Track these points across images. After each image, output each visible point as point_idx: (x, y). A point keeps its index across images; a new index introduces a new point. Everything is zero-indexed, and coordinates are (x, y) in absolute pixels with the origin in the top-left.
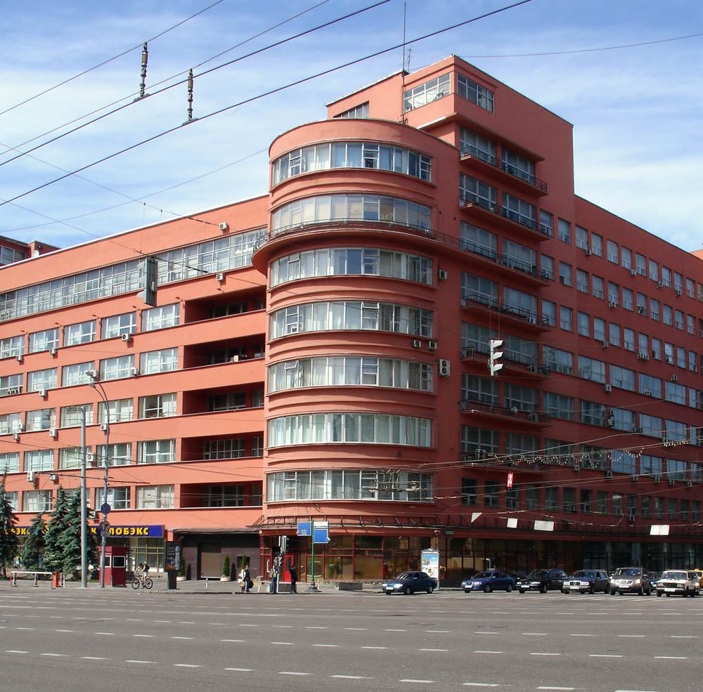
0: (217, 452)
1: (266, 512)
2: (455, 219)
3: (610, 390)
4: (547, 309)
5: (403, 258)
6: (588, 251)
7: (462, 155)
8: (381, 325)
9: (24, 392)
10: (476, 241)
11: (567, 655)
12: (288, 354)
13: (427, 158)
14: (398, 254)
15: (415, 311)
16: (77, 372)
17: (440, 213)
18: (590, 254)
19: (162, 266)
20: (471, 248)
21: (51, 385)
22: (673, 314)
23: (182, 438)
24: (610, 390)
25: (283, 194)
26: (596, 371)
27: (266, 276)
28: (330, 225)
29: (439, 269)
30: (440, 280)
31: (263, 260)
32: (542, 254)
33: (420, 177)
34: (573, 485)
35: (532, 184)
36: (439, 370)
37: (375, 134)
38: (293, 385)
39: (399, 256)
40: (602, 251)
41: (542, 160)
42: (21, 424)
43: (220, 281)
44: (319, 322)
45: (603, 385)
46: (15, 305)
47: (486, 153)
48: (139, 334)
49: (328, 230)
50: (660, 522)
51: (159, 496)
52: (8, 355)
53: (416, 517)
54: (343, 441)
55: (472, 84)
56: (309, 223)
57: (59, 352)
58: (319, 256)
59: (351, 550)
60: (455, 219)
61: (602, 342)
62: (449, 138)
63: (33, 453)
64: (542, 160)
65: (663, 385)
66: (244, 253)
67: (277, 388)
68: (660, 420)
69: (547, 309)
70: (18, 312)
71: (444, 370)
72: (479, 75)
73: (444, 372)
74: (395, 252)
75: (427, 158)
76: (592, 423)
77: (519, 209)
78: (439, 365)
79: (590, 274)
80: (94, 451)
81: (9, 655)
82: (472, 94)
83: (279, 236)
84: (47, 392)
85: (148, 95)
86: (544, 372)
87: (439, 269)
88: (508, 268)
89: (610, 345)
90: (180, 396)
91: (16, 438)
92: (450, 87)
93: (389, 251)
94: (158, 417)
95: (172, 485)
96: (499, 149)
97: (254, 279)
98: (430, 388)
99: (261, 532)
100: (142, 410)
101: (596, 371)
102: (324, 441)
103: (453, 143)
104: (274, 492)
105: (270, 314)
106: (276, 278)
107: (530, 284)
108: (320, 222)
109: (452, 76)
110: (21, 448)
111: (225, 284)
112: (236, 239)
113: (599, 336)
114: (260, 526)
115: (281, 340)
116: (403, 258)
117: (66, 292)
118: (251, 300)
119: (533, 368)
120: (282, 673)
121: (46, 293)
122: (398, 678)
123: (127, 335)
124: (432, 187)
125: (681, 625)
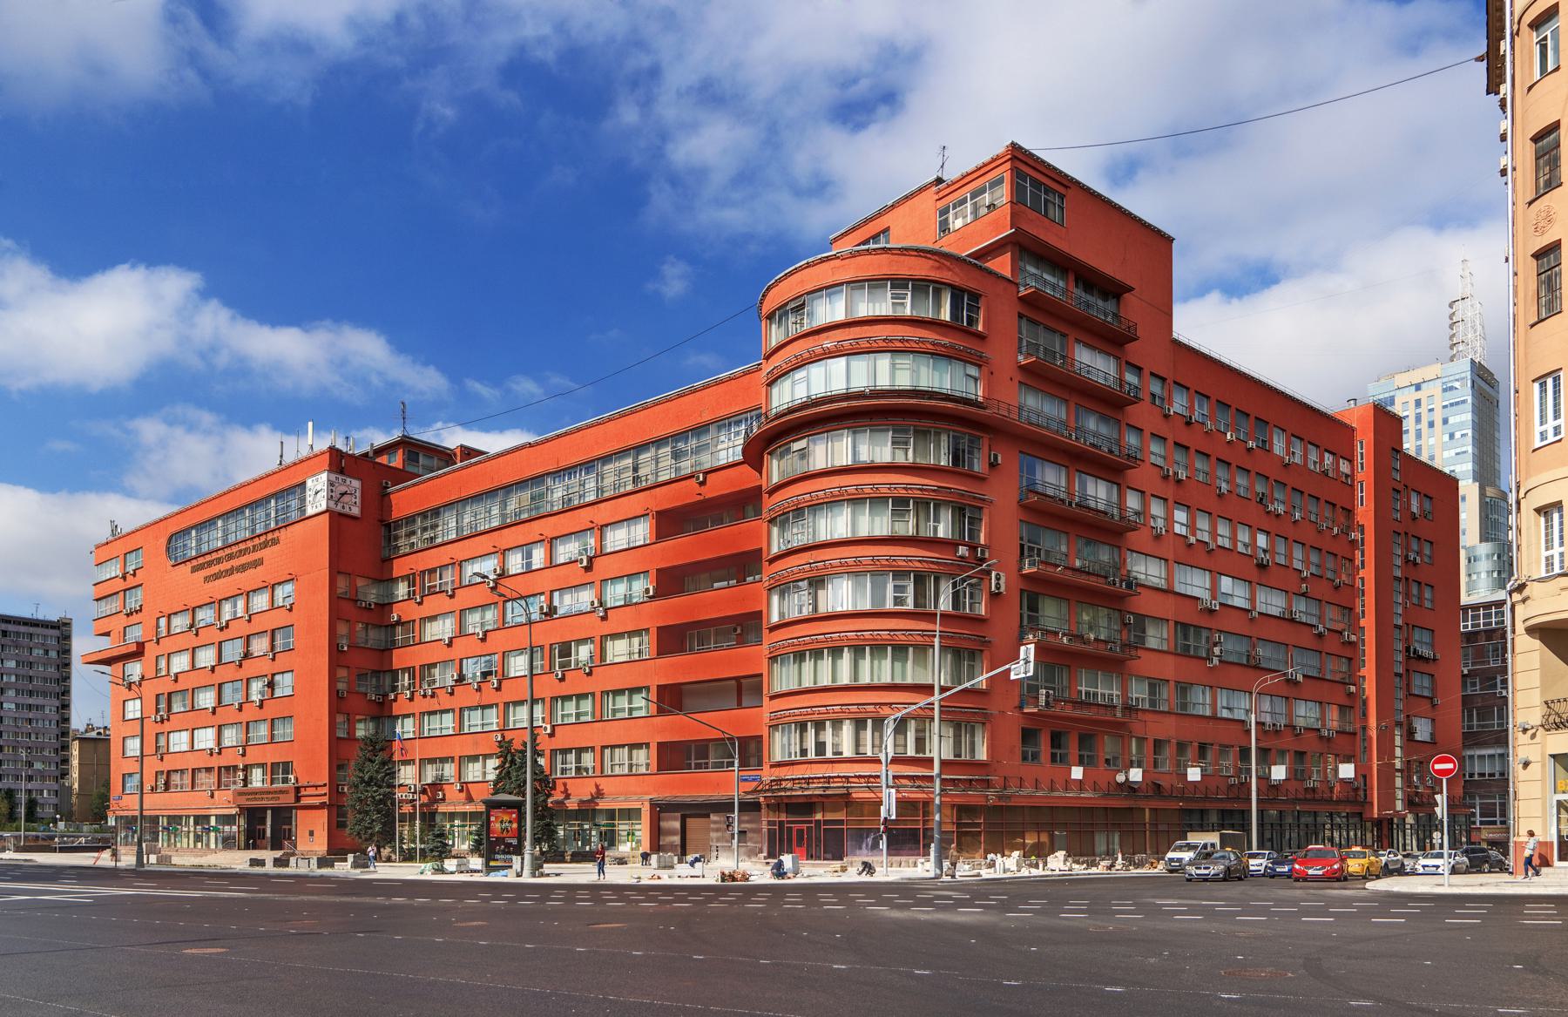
0: (1498, 801)
1: (767, 775)
2: (1011, 379)
3: (1217, 608)
4: (1133, 502)
5: (944, 438)
6: (1191, 417)
7: (1022, 289)
8: (873, 603)
9: (417, 640)
10: (1041, 409)
11: (594, 833)
12: (869, 693)
13: (975, 297)
14: (938, 288)
15: (960, 508)
16: (479, 761)
17: (992, 373)
18: (1193, 421)
19: (278, 636)
20: (1034, 419)
21: (752, 418)
22: (1288, 443)
23: (658, 686)
24: (1217, 608)
25: (970, 184)
26: (1195, 583)
27: (761, 473)
28: (847, 397)
29: (990, 450)
30: (993, 465)
31: (755, 453)
32: (1129, 487)
33: (965, 324)
34: (43, 629)
35: (1115, 326)
36: (990, 587)
37: (922, 268)
38: (800, 611)
39: (938, 434)
40: (1167, 580)
41: (1130, 289)
42: (455, 674)
43: (491, 588)
44: (849, 439)
45: (1318, 730)
46: (441, 523)
47: (1051, 284)
48: (468, 586)
49: (844, 404)
50: (992, 749)
51: (630, 758)
52: (794, 587)
53: (1279, 482)
54: (610, 718)
55: (1036, 184)
56: (818, 396)
57: (137, 571)
58: (562, 702)
59: (980, 832)
60: (1011, 379)
61: (1207, 543)
62: (1002, 264)
63: (473, 609)
64: (1130, 289)
65: (321, 806)
66: (728, 448)
67: (831, 535)
68: (1207, 573)
69: (1133, 502)
70: (1062, 489)
71: (998, 587)
72: (553, 659)
73: (998, 588)
74: (1470, 629)
75: (975, 297)
76: (1192, 653)
77: (1544, 35)
78: (991, 579)
79: (1423, 585)
80: (165, 776)
81: (223, 947)
82: (1036, 198)
83: (779, 416)
84: (485, 633)
85: (1559, 813)
86: (1129, 586)
87: (990, 450)
88: (1066, 507)
89: (1197, 540)
90: (654, 631)
91: (476, 687)
92: (1003, 195)
93: (979, 434)
94: (459, 464)
95: (453, 758)
96: (1071, 278)
97: (746, 478)
98: (982, 610)
99: (762, 799)
100: (509, 718)
101: (1195, 583)
102: (624, 773)
103: (1008, 273)
104: (781, 746)
105: (769, 521)
106: (776, 469)
107: (1113, 469)
108: (833, 393)
109: (1007, 176)
110: (455, 702)
111: (592, 571)
112: (1552, 843)
113: (1180, 515)
114: (760, 791)
115: (783, 554)
116: (944, 438)
117: (504, 505)
118: (745, 502)
119: (1114, 580)
120: (219, 950)
121: (480, 508)
122: (589, 952)
123: (585, 558)
124: (980, 337)
125: (1364, 728)
